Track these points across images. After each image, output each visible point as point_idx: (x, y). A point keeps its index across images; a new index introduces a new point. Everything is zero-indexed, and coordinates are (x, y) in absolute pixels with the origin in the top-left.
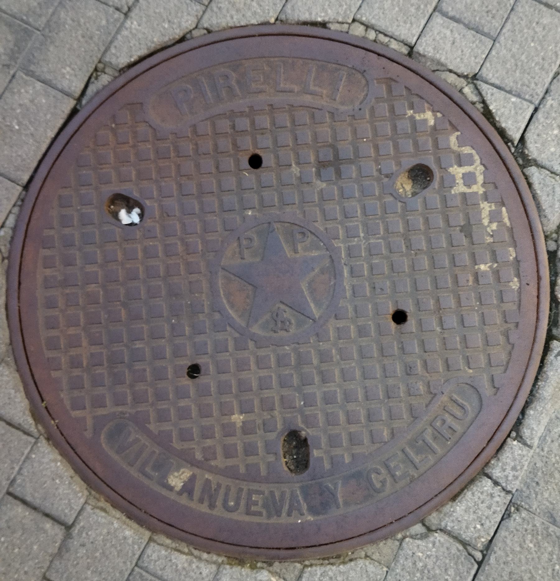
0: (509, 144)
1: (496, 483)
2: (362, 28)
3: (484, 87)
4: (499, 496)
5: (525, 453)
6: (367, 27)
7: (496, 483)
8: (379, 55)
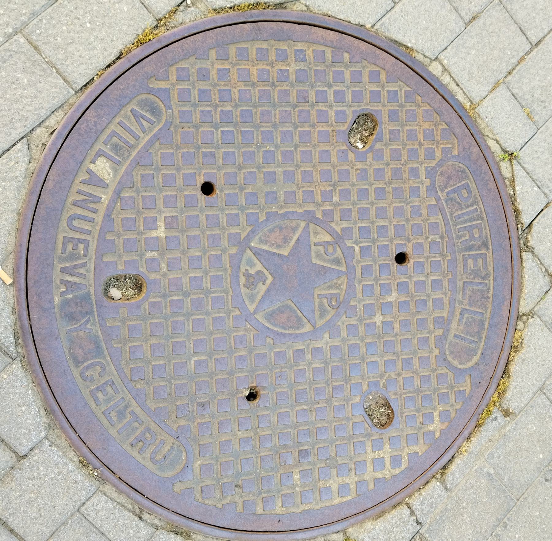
0: (519, 226)
1: (412, 513)
2: (440, 68)
3: (516, 167)
4: (412, 525)
5: (442, 494)
6: (445, 70)
7: (412, 513)
8: (266, 532)
